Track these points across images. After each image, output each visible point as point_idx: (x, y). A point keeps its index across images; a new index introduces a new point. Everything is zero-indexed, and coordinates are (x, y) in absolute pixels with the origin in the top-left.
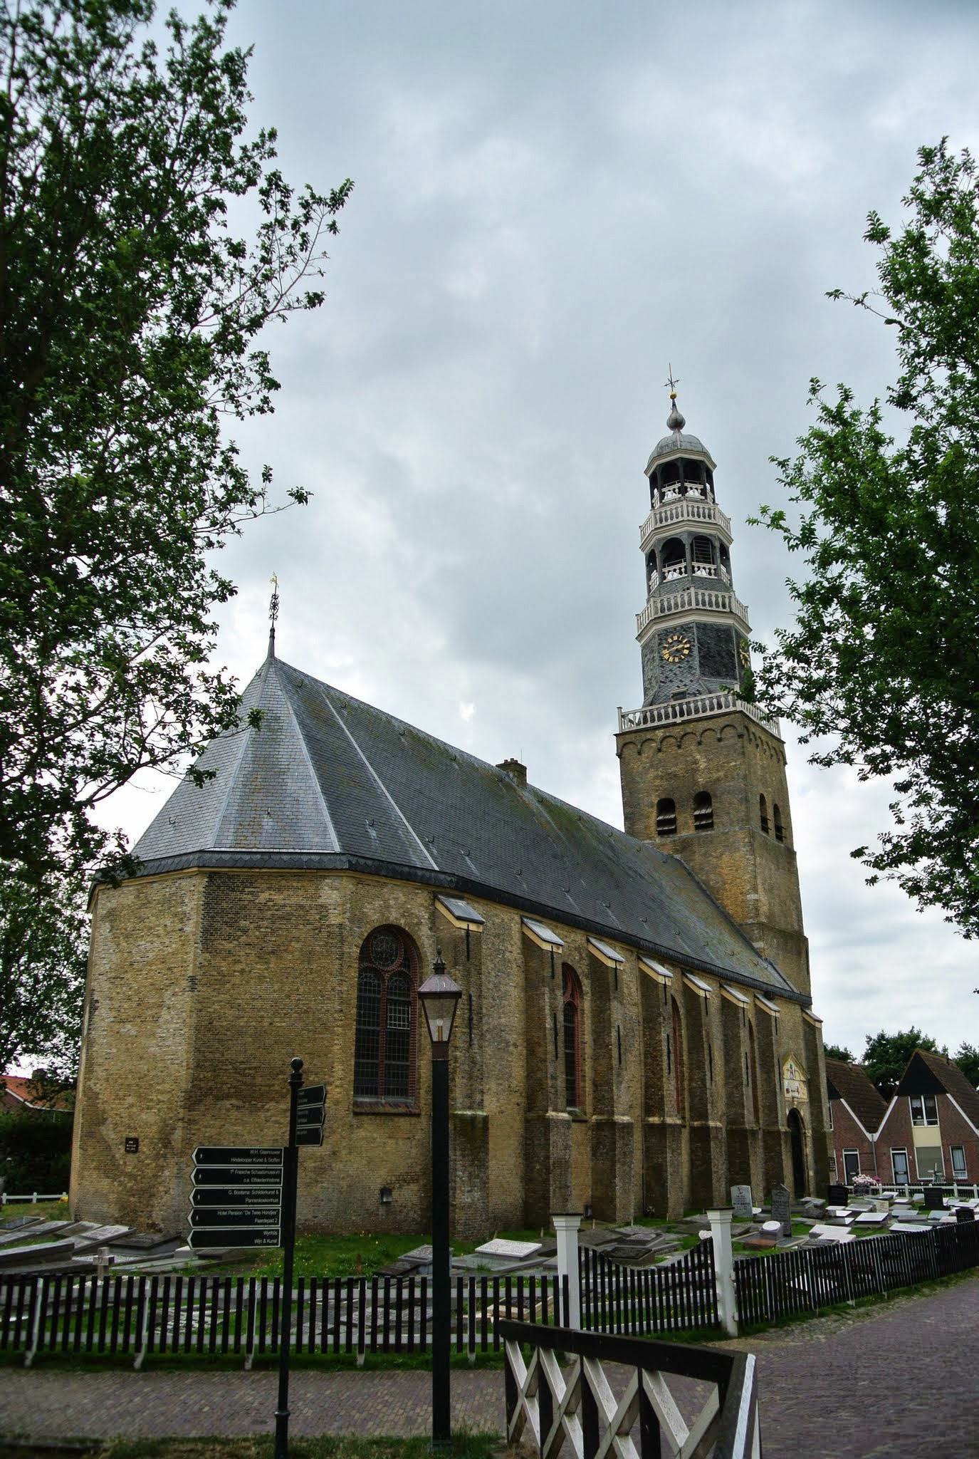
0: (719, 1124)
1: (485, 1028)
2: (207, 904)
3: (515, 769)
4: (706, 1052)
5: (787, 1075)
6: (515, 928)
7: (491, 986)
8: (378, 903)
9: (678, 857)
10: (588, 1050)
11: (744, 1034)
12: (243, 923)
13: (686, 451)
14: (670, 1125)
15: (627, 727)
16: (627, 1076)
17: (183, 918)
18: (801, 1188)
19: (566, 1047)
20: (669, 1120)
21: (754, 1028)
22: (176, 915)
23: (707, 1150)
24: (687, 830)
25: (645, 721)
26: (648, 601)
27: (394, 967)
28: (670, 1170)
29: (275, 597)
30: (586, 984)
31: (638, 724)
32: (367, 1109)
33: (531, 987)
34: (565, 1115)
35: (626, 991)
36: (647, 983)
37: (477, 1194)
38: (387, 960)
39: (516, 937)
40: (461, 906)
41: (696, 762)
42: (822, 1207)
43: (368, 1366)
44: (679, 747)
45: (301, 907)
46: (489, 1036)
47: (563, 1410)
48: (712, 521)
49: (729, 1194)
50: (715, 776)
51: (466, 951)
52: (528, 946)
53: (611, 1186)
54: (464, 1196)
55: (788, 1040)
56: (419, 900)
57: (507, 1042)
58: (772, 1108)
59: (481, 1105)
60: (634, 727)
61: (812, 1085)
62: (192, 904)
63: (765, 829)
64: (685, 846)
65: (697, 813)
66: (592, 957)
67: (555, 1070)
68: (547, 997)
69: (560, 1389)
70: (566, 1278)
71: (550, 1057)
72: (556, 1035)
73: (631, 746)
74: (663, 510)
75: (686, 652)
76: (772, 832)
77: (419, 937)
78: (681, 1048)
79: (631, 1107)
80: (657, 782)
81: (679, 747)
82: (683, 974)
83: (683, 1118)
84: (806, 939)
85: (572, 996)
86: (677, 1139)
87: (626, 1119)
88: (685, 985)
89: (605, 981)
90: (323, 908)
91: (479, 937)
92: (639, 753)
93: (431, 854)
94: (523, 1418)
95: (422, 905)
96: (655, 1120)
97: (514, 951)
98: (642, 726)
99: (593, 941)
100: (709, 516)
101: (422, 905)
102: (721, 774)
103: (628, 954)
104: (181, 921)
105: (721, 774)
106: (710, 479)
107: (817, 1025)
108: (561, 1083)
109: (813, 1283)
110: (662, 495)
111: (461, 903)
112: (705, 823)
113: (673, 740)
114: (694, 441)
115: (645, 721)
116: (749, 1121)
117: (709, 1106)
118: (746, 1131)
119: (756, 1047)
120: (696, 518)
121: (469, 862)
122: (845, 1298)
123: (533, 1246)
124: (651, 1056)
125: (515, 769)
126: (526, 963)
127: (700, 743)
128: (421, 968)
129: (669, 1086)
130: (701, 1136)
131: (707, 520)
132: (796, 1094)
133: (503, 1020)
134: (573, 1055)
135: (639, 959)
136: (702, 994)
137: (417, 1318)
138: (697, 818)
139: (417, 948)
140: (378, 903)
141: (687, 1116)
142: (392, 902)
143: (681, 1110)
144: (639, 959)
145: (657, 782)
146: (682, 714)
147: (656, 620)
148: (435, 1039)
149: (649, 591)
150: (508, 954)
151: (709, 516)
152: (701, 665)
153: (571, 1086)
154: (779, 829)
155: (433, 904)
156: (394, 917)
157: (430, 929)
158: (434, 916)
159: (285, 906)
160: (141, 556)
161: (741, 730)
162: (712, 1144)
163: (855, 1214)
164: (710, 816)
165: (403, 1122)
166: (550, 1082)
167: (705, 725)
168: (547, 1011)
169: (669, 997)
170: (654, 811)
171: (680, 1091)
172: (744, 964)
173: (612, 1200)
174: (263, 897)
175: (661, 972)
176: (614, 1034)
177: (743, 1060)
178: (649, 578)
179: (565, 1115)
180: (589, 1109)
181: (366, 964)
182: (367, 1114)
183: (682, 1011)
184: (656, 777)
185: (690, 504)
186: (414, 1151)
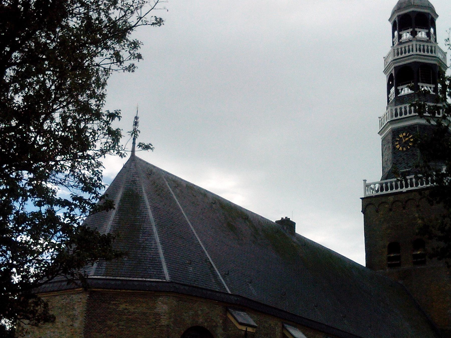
2: (88, 310)
3: (287, 225)
6: (278, 330)
8: (191, 313)
12: (109, 323)
13: (418, 6)
15: (370, 193)
17: (73, 318)
22: (69, 316)
25: (382, 190)
29: (136, 118)
31: (377, 191)
40: (243, 317)
44: (404, 208)
45: (144, 314)
48: (433, 55)
60: (374, 194)
62: (79, 310)
74: (400, 47)
81: (404, 208)
90: (157, 315)
92: (377, 211)
98: (380, 193)
100: (432, 52)
104: (72, 320)
110: (400, 36)
111: (242, 314)
120: (422, 53)
121: (251, 287)
125: (287, 225)
131: (430, 54)
138: (415, 256)
140: (191, 313)
142: (200, 312)
147: (392, 122)
149: (388, 101)
155: (226, 314)
157: (223, 330)
159: (134, 313)
160: (87, 205)
170: (386, 250)
174: (122, 306)
178: (389, 92)
185: (418, 43)
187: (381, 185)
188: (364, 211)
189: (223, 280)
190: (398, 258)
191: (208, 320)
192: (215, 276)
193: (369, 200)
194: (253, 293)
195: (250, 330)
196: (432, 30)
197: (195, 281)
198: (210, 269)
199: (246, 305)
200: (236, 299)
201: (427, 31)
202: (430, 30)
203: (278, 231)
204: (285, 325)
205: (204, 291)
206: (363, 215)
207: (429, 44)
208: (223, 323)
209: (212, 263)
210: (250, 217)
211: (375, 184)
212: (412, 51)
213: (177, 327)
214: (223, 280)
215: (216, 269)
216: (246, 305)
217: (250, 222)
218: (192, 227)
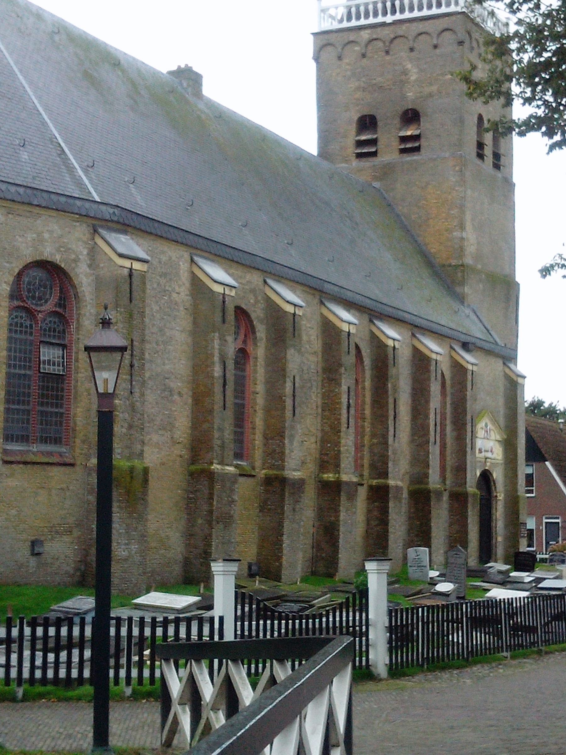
0: (400, 483)
1: (147, 375)
3: (188, 78)
4: (391, 406)
5: (480, 433)
6: (184, 266)
7: (155, 330)
8: (31, 236)
9: (377, 184)
10: (260, 400)
11: (435, 388)
14: (347, 483)
16: (300, 429)
18: (486, 553)
19: (236, 397)
20: (345, 478)
21: (448, 382)
23: (385, 511)
24: (389, 152)
25: (349, 19)
27: (49, 306)
28: (342, 529)
30: (261, 331)
31: (341, 21)
32: (18, 458)
33: (200, 331)
34: (231, 469)
35: (305, 338)
36: (330, 331)
37: (134, 547)
38: (40, 299)
39: (185, 277)
40: (125, 243)
41: (405, 72)
42: (506, 573)
43: (25, 698)
44: (387, 52)
46: (151, 383)
47: (210, 706)
49: (405, 558)
50: (427, 90)
51: (130, 289)
52: (198, 287)
53: (278, 544)
54: (121, 548)
55: (485, 396)
56: (77, 234)
57: (171, 391)
58: (461, 469)
59: (141, 455)
60: (336, 26)
61: (509, 445)
63: (481, 156)
64: (386, 172)
65: (402, 134)
66: (268, 299)
67: (223, 426)
68: (216, 343)
69: (208, 691)
70: (221, 619)
71: (218, 407)
72: (224, 386)
73: (330, 49)
76: (489, 158)
77: (77, 275)
78: (364, 402)
79: (303, 463)
80: (359, 95)
81: (387, 52)
82: (371, 321)
83: (361, 476)
85: (244, 342)
86: (352, 497)
87: (297, 475)
88: (372, 333)
89: (283, 328)
91: (143, 276)
92: (340, 58)
93: (91, 181)
94: (176, 722)
95: (79, 239)
96: (329, 476)
97: (182, 293)
98: (345, 24)
99: (270, 282)
101: (79, 239)
102: (434, 88)
103: (310, 298)
105: (434, 88)
107: (520, 380)
108: (228, 435)
109: (469, 637)
111: (123, 238)
112: (411, 146)
113: (380, 44)
115: (349, 19)
116: (434, 480)
117: (390, 464)
118: (429, 491)
119: (448, 399)
121: (133, 190)
122: (499, 649)
123: (192, 599)
124: (330, 406)
125: (188, 78)
126: (195, 306)
127: (412, 50)
128: (78, 308)
129: (348, 441)
130: (380, 495)
132: (489, 455)
133: (167, 367)
134: (243, 406)
135: (322, 303)
136: (390, 343)
137: (75, 659)
138: (404, 139)
139: (74, 287)
141: (366, 473)
142: (46, 236)
143: (358, 467)
144: (322, 303)
145: (359, 95)
148: (101, 390)
150: (174, 295)
153: (240, 437)
154: (497, 156)
156: (49, 252)
157: (90, 266)
158: (93, 251)
161: (462, 35)
162: (391, 504)
163: (539, 580)
164: (416, 138)
165: (56, 471)
166: (216, 434)
167: (421, 27)
168: (216, 359)
169: (352, 347)
170: (353, 128)
171: (359, 447)
172: (440, 313)
173: (279, 558)
175: (345, 318)
176: (289, 385)
177: (432, 416)
179: (231, 469)
180: (258, 464)
181: (16, 303)
182: (19, 463)
183: (367, 362)
184: (358, 89)
186: (68, 502)
188: (317, 58)
189: (84, 178)
190: (373, 142)
191: (62, 249)
192: (71, 170)
193: (326, 36)
194: (139, 201)
195: (137, 266)
197: (34, 178)
198: (59, 155)
199: (129, 222)
200: (111, 211)
203: (172, 91)
204: (195, 258)
205: (53, 196)
208: (88, 254)
209: (63, 145)
210: (122, 62)
213: (7, 262)
214: (84, 178)
215: (71, 157)
216: (129, 222)
217: (123, 71)
218: (21, 77)
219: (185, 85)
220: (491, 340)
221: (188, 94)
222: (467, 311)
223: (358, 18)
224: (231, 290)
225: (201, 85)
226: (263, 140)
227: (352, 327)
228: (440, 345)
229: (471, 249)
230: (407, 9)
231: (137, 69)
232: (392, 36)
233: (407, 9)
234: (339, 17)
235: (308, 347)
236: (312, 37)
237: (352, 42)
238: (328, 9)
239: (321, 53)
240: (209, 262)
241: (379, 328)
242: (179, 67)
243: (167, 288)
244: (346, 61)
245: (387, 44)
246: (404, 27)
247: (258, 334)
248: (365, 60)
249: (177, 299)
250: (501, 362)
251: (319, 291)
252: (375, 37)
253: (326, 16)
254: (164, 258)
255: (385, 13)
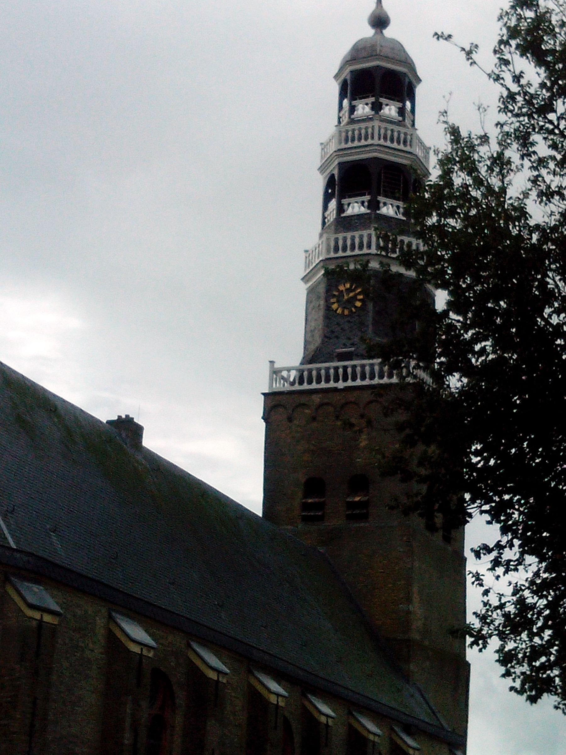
3: (128, 429)
6: (100, 622)
13: (387, 58)
15: (279, 386)
25: (301, 382)
26: (321, 236)
30: (181, 697)
31: (293, 384)
36: (256, 700)
39: (101, 632)
48: (408, 149)
60: (287, 387)
73: (281, 410)
74: (350, 127)
75: (358, 304)
84: (468, 665)
88: (304, 707)
91: (53, 629)
97: (95, 650)
98: (297, 387)
100: (405, 143)
106: (412, 97)
110: (352, 109)
111: (36, 588)
113: (331, 409)
114: (398, 47)
121: (54, 539)
131: (401, 147)
138: (352, 505)
146: (345, 379)
149: (324, 223)
150: (87, 652)
151: (405, 143)
152: (375, 323)
178: (325, 208)
183: (297, 739)
185: (384, 125)
187: (301, 372)
188: (266, 418)
190: (320, 506)
193: (277, 398)
195: (47, 618)
196: (408, 104)
200: (25, 558)
201: (400, 105)
202: (404, 105)
204: (114, 614)
206: (264, 424)
207: (402, 130)
211: (289, 370)
212: (373, 138)
217: (59, 416)
219: (124, 435)
220: (436, 723)
221: (126, 444)
222: (412, 690)
223: (310, 382)
224: (149, 651)
225: (142, 437)
226: (202, 496)
227: (280, 699)
228: (378, 726)
229: (418, 624)
230: (323, 379)
231: (75, 417)
232: (343, 401)
233: (323, 379)
234: (292, 379)
235: (232, 718)
236: (263, 396)
237: (304, 404)
238: (281, 371)
239: (273, 413)
240: (126, 619)
241: (311, 702)
242: (120, 417)
243: (80, 644)
244: (296, 422)
245: (290, 411)
246: (356, 393)
247: (178, 701)
248: (315, 424)
249: (89, 656)
250: (446, 750)
251: (247, 659)
252: (326, 401)
253: (278, 378)
254: (79, 612)
255: (336, 380)
